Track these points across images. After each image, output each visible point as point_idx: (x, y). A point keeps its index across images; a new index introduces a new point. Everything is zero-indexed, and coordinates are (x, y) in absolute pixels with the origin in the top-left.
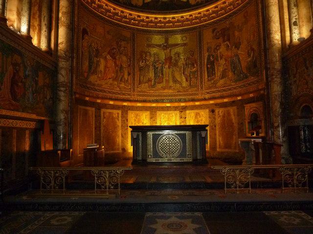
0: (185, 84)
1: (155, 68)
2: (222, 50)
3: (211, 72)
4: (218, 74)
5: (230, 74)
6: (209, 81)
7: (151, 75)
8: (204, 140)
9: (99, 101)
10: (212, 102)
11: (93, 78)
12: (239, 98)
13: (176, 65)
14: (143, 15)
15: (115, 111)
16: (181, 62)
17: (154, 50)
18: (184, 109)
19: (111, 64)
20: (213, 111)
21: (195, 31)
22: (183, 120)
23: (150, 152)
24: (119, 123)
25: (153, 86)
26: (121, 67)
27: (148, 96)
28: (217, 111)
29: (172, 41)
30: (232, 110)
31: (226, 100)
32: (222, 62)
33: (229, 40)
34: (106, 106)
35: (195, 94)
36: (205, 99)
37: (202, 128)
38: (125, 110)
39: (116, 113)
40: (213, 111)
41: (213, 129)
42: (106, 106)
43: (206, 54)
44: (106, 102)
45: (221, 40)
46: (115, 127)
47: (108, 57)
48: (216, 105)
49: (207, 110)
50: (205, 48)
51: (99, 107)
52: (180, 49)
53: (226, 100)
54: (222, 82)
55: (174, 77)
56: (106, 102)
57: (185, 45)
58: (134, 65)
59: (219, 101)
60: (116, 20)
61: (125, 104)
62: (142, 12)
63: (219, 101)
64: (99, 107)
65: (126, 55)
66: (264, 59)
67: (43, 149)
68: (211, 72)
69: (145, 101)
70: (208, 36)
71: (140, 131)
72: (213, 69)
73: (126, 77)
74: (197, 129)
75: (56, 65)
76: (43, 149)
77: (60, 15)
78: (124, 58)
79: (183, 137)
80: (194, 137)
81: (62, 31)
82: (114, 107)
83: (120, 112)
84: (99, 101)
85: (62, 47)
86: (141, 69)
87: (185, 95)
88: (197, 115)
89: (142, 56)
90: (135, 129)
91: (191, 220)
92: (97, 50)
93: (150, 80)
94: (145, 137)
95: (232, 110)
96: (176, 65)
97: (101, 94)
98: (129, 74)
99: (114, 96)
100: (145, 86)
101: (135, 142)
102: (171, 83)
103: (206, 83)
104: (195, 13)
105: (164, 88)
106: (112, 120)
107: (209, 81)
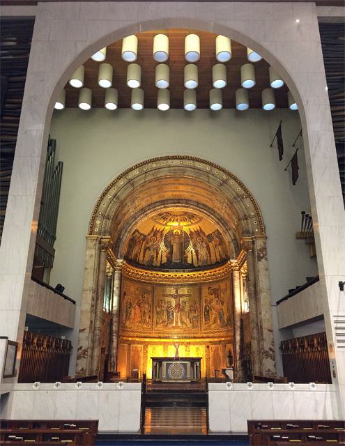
0: (190, 325)
1: (168, 312)
2: (214, 303)
3: (207, 319)
4: (212, 320)
5: (219, 321)
6: (206, 324)
7: (165, 317)
8: (198, 368)
9: (130, 339)
10: (207, 340)
11: (128, 324)
12: (223, 339)
13: (182, 310)
14: (160, 273)
15: (138, 346)
16: (187, 309)
17: (167, 299)
18: (189, 343)
19: (138, 311)
20: (208, 347)
21: (197, 286)
22: (187, 352)
23: (164, 376)
24: (142, 355)
25: (166, 326)
26: (144, 313)
27: (162, 333)
28: (210, 346)
29: (180, 292)
30: (220, 347)
31: (216, 340)
32: (214, 312)
33: (218, 297)
34: (134, 342)
35: (197, 333)
36: (203, 338)
37: (199, 359)
38: (146, 345)
39: (140, 347)
40: (208, 347)
41: (208, 360)
42: (134, 342)
43: (204, 305)
44: (134, 339)
45: (213, 296)
46: (139, 357)
47: (137, 307)
48: (210, 342)
49: (204, 346)
50: (203, 299)
51: (130, 343)
52: (185, 299)
53: (216, 340)
54: (213, 326)
55: (181, 319)
56: (134, 339)
57: (190, 295)
58: (153, 311)
59: (211, 340)
60: (143, 279)
61: (146, 340)
62: (160, 271)
63: (211, 340)
64: (130, 343)
65: (148, 304)
66: (182, 354)
67: (109, 371)
68: (207, 319)
69: (160, 338)
70: (205, 291)
71: (158, 361)
72: (209, 316)
73: (147, 320)
74: (194, 361)
75: (112, 320)
76: (109, 371)
77: (115, 289)
78: (147, 306)
79: (185, 365)
80: (192, 365)
81: (116, 299)
82: (139, 343)
83: (142, 346)
84: (130, 339)
85: (115, 309)
86: (158, 313)
87: (189, 333)
88: (198, 349)
89: (159, 303)
90: (154, 359)
91: (147, 251)
92: (131, 304)
93: (164, 322)
94: (161, 365)
95: (220, 347)
96: (182, 310)
97: (131, 334)
98: (149, 318)
99: (139, 335)
100: (160, 327)
101: (154, 368)
102: (179, 324)
103: (204, 327)
104: (197, 274)
105: (174, 328)
106: (137, 352)
107: (206, 324)
